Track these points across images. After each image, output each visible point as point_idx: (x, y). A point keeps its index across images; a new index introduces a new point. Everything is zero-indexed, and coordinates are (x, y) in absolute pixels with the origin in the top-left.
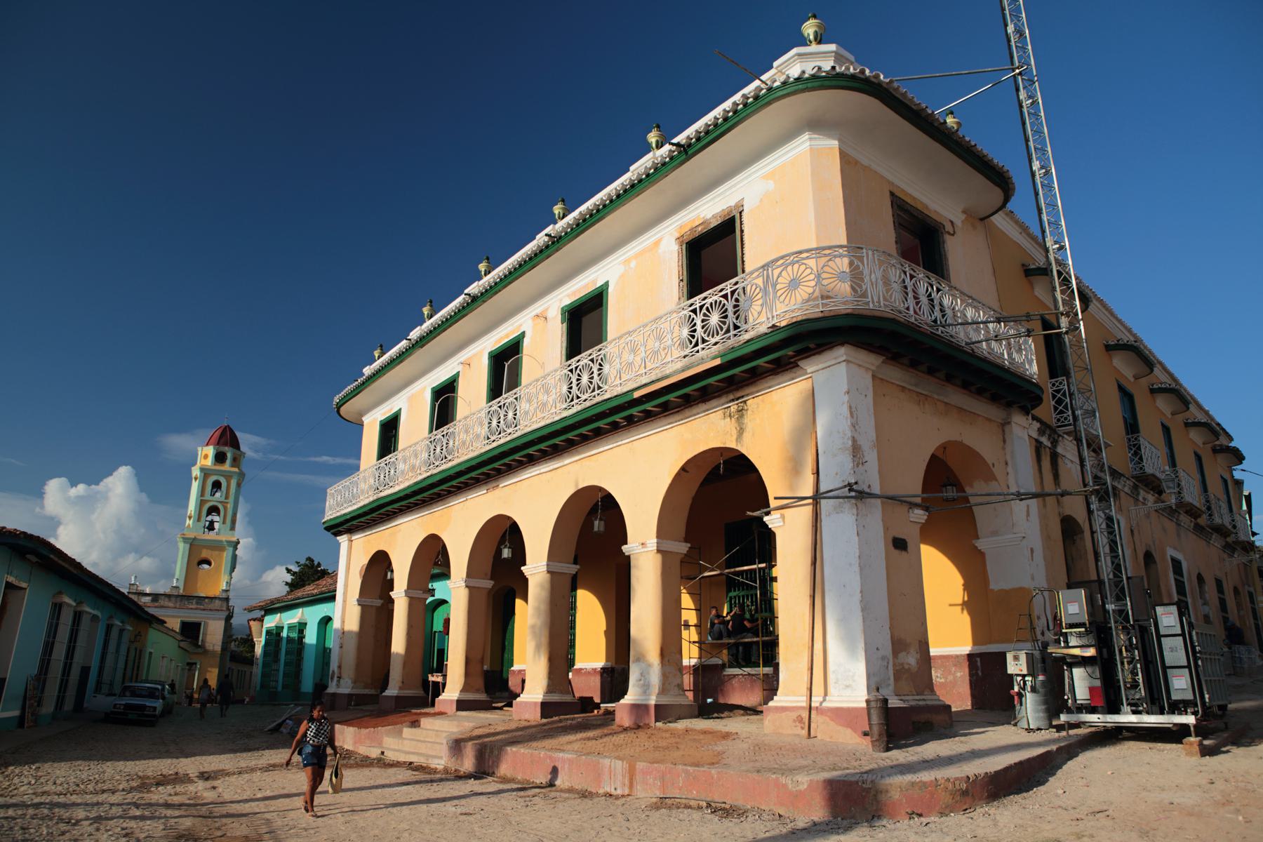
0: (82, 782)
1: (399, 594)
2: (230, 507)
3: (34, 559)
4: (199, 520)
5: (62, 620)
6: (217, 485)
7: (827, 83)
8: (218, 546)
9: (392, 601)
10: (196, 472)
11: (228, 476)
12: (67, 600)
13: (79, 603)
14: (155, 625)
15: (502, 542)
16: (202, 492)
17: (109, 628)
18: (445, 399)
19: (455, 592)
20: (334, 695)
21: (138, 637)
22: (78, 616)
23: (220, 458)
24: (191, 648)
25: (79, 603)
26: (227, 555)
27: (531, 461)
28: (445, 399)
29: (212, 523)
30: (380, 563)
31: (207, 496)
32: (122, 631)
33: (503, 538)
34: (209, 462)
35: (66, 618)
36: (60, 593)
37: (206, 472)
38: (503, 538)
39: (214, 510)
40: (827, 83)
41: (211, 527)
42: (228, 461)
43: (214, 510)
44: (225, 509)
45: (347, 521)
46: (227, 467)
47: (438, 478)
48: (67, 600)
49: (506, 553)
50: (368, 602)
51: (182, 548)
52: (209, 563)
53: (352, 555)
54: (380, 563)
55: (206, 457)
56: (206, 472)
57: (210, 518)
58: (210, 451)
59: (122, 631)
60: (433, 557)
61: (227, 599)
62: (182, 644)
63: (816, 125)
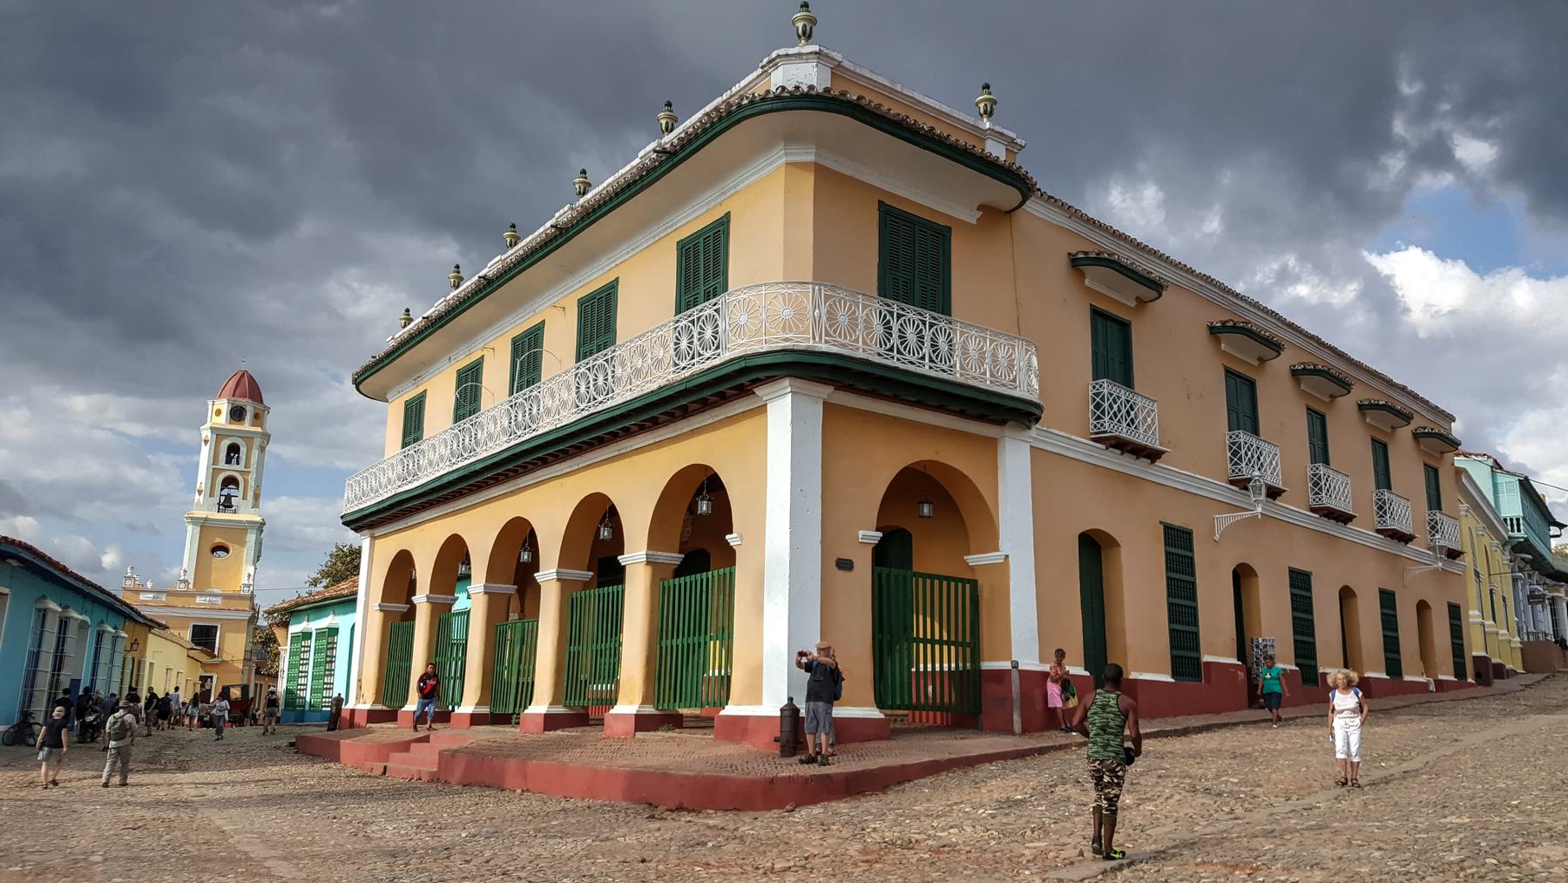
0: (87, 802)
1: (421, 598)
2: (251, 478)
3: (14, 563)
4: (211, 495)
5: (47, 628)
6: (234, 449)
7: (792, 105)
8: (240, 529)
9: (537, 588)
10: (206, 433)
11: (249, 437)
12: (53, 606)
13: (66, 607)
14: (156, 630)
15: (699, 493)
16: (215, 460)
17: (100, 635)
18: (470, 380)
19: (472, 600)
20: (353, 712)
21: (137, 644)
22: (64, 624)
23: (237, 414)
24: (205, 659)
25: (66, 607)
26: (251, 538)
27: (544, 463)
28: (470, 380)
29: (228, 497)
30: (403, 564)
31: (222, 464)
32: (115, 638)
33: (519, 536)
34: (222, 421)
35: (52, 627)
36: (44, 597)
37: (219, 434)
38: (519, 536)
39: (230, 481)
40: (792, 105)
41: (227, 504)
42: (249, 417)
43: (230, 481)
44: (246, 481)
45: (366, 516)
46: (246, 426)
47: (455, 476)
48: (53, 606)
49: (704, 507)
50: (393, 606)
51: (192, 532)
52: (226, 550)
53: (376, 555)
54: (403, 564)
55: (218, 413)
56: (219, 434)
57: (225, 492)
58: (224, 405)
59: (115, 638)
60: (454, 554)
61: (252, 598)
62: (192, 653)
63: (792, 138)
